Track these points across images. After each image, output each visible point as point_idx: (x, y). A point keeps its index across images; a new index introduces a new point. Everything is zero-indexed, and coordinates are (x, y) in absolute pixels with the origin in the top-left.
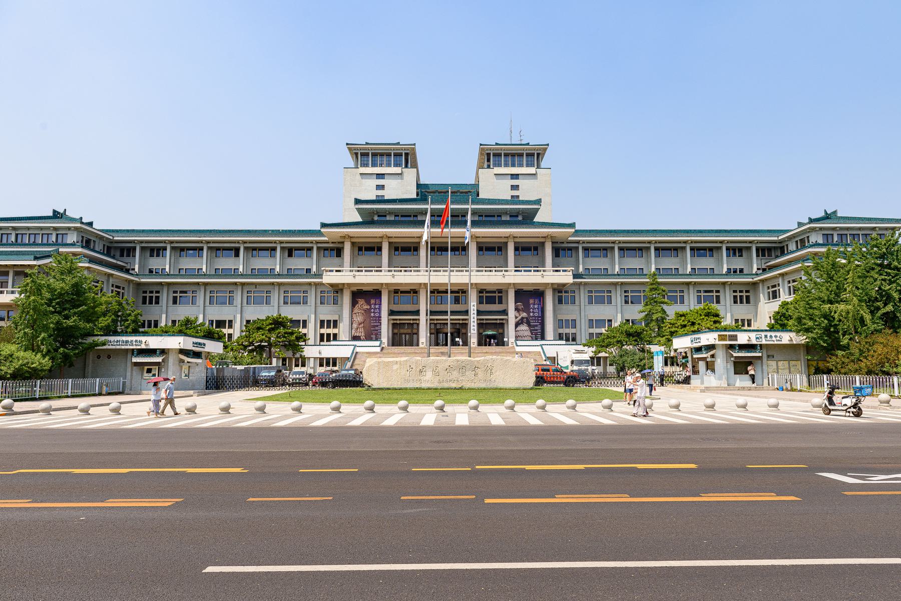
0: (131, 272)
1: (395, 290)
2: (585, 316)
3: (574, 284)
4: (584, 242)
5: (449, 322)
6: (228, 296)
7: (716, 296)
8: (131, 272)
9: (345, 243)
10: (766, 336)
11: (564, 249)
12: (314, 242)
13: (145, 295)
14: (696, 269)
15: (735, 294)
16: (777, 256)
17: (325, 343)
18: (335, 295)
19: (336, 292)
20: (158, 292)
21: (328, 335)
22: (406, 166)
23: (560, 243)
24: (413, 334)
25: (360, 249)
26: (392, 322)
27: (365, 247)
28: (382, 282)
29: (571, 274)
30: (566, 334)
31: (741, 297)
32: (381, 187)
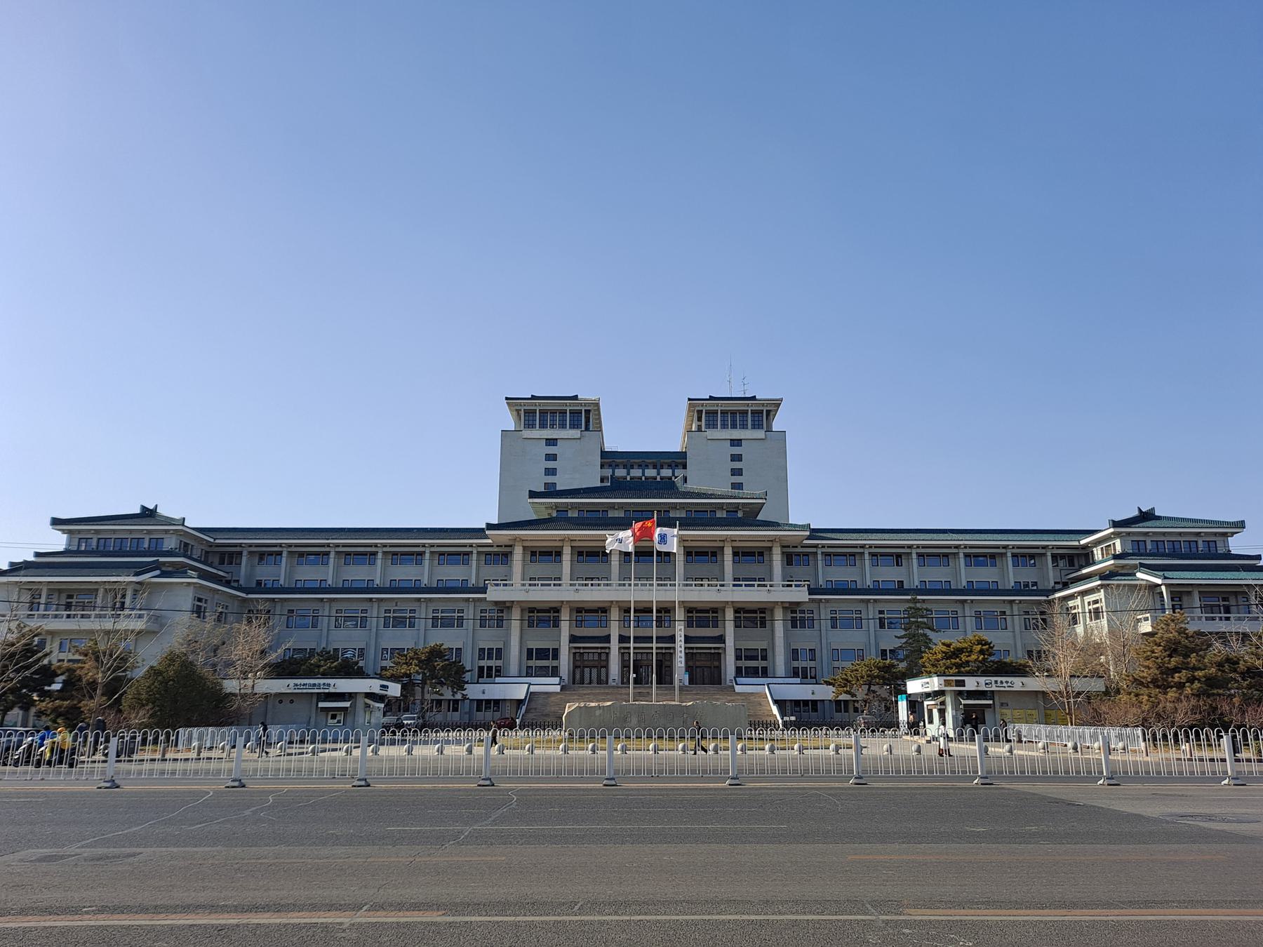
0: (232, 584)
1: (529, 608)
2: (827, 644)
3: (812, 601)
4: (823, 547)
5: (654, 651)
8: (232, 584)
9: (774, 549)
10: (996, 682)
11: (798, 554)
12: (474, 545)
14: (927, 583)
16: (1082, 565)
17: (485, 679)
18: (499, 615)
21: (490, 668)
22: (587, 429)
23: (793, 547)
24: (602, 667)
25: (533, 554)
26: (574, 651)
27: (540, 552)
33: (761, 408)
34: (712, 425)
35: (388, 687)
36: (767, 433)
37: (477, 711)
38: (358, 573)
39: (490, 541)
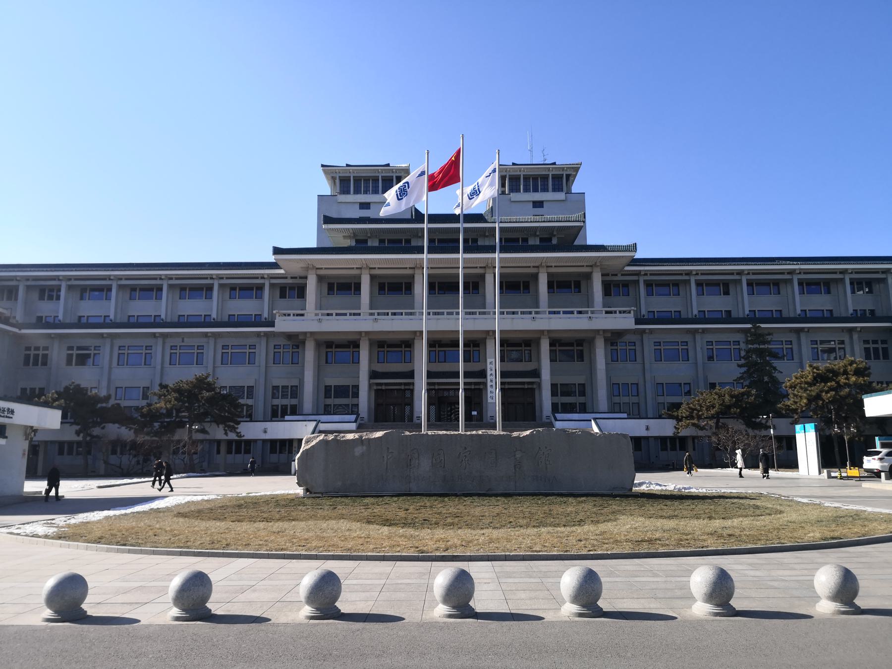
3: (635, 331)
6: (144, 354)
7: (883, 348)
9: (310, 277)
13: (28, 352)
15: (867, 346)
19: (296, 346)
20: (46, 348)
23: (613, 275)
24: (406, 404)
26: (375, 387)
28: (489, 329)
29: (633, 316)
30: (282, 406)
31: (876, 350)
32: (365, 206)
33: (561, 173)
34: (514, 189)
35: (12, 412)
36: (567, 195)
37: (271, 452)
38: (143, 308)
39: (282, 271)
